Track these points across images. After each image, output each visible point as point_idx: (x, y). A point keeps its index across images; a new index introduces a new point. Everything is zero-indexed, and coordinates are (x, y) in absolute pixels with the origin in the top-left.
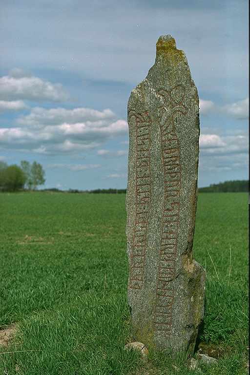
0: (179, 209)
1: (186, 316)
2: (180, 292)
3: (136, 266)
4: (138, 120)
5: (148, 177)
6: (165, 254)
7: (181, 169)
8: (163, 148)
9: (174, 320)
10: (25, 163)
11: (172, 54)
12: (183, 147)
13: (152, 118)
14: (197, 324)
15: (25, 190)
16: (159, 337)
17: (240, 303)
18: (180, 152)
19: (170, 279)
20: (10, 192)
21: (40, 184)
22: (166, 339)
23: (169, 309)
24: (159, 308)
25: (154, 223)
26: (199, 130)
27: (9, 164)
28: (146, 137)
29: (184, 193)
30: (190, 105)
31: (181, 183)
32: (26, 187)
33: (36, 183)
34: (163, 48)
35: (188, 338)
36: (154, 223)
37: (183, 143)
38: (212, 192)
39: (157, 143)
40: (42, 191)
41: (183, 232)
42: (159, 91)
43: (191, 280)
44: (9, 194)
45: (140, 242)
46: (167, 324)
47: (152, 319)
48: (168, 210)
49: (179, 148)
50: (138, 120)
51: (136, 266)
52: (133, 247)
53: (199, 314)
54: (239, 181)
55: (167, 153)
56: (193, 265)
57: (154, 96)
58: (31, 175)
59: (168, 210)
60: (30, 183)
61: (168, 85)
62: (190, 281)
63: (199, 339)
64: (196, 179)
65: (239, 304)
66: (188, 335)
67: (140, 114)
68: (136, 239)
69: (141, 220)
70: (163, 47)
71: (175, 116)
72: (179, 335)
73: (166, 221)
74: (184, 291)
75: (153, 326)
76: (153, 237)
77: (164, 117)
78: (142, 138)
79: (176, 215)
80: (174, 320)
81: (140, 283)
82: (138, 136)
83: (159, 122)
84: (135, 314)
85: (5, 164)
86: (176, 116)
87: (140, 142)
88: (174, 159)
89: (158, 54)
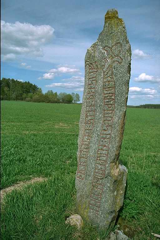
0: (111, 130)
1: (110, 205)
2: (107, 188)
3: (81, 164)
4: (90, 68)
5: (94, 106)
6: (100, 160)
7: (115, 102)
8: (104, 87)
9: (102, 206)
10: (73, 93)
11: (115, 21)
12: (118, 87)
13: (99, 66)
14: (117, 210)
15: (73, 103)
16: (91, 214)
17: (149, 189)
18: (115, 91)
19: (101, 178)
20: (68, 103)
21: (78, 101)
22: (96, 216)
23: (99, 198)
24: (93, 195)
25: (95, 138)
26: (130, 75)
27: (68, 94)
28: (94, 79)
29: (116, 119)
30: (125, 57)
31: (114, 112)
32: (73, 102)
33: (77, 101)
34: (109, 18)
35: (110, 220)
36: (95, 138)
37: (118, 84)
38: (141, 108)
39: (100, 83)
40: (79, 104)
41: (113, 147)
42: (104, 47)
43: (115, 181)
44: (66, 104)
45: (85, 149)
46: (97, 207)
47: (88, 201)
48: (104, 130)
49: (114, 87)
50: (90, 68)
51: (81, 164)
52: (81, 151)
53: (120, 202)
54: (150, 104)
55: (106, 91)
56: (118, 170)
57: (101, 51)
58: (75, 98)
59: (104, 130)
60: (75, 101)
61: (111, 43)
62: (115, 181)
63: (118, 217)
64: (125, 110)
65: (148, 190)
66: (110, 218)
67: (92, 64)
68: (83, 146)
69: (87, 134)
70: (109, 17)
71: (114, 65)
72: (104, 217)
73: (102, 138)
74: (110, 188)
75: (89, 205)
76: (93, 147)
77: (107, 66)
78: (91, 80)
79: (109, 134)
80: (102, 206)
81: (83, 176)
82: (89, 79)
83: (103, 69)
84: (78, 195)
85: (66, 94)
86: (115, 64)
87: (90, 82)
88: (111, 95)
89: (105, 22)
